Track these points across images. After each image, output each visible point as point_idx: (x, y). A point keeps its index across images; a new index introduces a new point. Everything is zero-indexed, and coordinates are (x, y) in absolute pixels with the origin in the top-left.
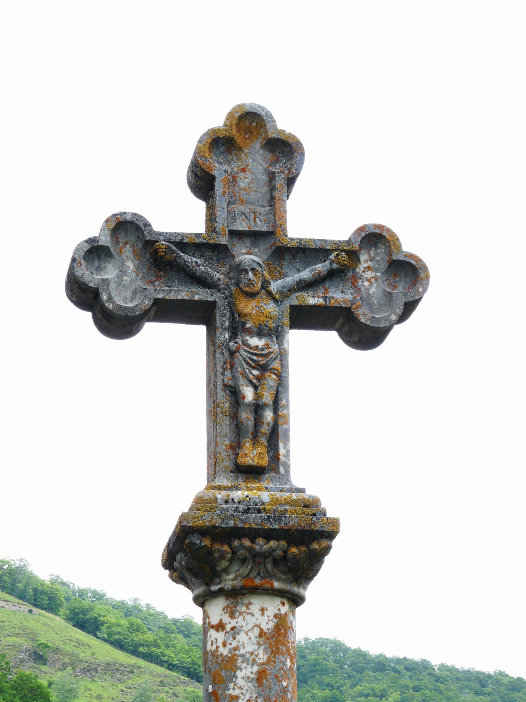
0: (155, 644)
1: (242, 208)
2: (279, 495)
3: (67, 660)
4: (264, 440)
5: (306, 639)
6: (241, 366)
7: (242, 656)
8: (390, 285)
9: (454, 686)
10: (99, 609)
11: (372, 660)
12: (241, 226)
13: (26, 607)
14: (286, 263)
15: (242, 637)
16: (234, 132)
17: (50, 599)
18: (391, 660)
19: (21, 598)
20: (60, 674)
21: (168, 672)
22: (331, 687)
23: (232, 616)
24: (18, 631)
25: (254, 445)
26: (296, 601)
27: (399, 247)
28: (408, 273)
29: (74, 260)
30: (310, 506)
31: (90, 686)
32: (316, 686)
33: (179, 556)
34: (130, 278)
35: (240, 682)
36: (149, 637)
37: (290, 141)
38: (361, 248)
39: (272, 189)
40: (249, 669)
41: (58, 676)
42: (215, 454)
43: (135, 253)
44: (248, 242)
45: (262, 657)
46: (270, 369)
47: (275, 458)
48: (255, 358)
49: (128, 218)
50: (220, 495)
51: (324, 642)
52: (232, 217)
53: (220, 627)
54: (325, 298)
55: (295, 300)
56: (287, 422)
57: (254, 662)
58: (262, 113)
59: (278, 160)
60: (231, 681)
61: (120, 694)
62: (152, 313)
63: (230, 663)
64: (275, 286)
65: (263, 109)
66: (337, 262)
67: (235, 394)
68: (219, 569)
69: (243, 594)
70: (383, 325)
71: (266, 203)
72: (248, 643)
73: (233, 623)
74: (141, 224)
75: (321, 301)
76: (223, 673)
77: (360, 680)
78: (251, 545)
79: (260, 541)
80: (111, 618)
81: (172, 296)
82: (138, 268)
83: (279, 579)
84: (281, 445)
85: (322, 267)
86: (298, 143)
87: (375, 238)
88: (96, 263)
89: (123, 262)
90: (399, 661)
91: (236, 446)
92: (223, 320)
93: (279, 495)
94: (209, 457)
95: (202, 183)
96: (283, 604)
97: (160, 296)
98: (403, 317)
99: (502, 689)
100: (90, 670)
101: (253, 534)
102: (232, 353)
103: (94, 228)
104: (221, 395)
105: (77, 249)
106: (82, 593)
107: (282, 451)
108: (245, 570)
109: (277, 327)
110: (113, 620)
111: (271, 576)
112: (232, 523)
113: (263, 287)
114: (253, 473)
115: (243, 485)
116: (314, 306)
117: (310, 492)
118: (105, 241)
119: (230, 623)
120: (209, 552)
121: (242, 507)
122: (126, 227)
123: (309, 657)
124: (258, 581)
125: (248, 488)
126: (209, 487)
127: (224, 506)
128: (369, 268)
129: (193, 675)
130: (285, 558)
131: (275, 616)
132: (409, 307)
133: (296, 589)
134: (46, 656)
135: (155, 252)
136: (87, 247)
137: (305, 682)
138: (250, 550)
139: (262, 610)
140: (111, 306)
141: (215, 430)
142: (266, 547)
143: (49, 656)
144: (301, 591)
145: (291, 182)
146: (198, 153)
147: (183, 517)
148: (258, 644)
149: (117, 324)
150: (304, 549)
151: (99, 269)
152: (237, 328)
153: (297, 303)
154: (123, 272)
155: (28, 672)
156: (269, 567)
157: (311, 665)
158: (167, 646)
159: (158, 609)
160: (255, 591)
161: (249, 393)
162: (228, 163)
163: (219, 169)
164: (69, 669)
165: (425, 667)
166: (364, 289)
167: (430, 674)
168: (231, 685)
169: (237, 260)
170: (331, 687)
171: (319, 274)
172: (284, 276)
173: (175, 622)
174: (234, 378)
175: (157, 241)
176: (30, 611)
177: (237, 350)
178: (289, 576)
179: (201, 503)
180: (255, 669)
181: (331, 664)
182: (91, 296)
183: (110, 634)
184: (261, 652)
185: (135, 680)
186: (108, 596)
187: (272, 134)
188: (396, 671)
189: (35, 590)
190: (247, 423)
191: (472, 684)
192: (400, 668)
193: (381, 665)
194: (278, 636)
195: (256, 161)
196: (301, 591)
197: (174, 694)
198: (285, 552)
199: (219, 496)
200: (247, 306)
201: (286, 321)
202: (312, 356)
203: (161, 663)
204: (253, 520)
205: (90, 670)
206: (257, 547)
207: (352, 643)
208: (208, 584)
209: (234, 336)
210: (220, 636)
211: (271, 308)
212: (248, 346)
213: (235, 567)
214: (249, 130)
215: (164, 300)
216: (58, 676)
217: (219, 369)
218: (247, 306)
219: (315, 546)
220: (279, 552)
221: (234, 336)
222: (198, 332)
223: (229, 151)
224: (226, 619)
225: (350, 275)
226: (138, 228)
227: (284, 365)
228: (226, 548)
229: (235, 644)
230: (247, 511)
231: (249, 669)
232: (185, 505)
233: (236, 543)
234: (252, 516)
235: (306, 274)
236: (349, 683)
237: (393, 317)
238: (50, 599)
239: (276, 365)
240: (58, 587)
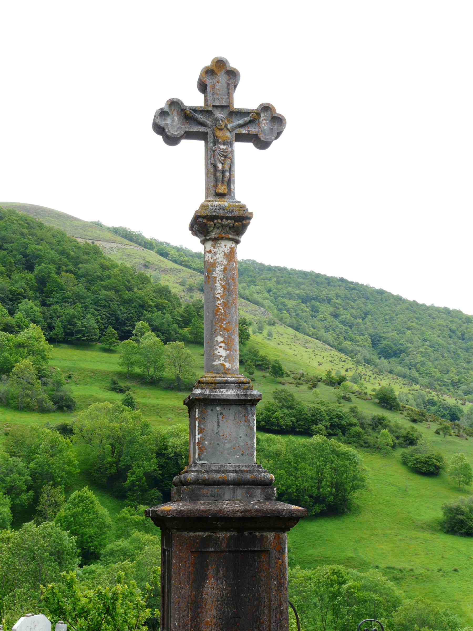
0: (188, 261)
1: (217, 96)
2: (231, 203)
3: (156, 267)
4: (226, 183)
5: (242, 259)
6: (217, 156)
7: (218, 262)
8: (272, 126)
9: (296, 276)
10: (168, 249)
11: (266, 267)
12: (217, 103)
13: (142, 248)
14: (233, 117)
15: (218, 255)
16: (214, 68)
17: (150, 245)
18: (273, 267)
19: (140, 245)
20: (154, 272)
21: (193, 271)
22: (251, 276)
23: (214, 248)
24: (139, 257)
25: (222, 185)
26: (237, 242)
27: (275, 112)
28: (278, 121)
29: (155, 116)
30: (243, 207)
31: (165, 277)
32: (246, 276)
33: (195, 226)
34: (176, 123)
35: (217, 272)
36: (186, 259)
37: (235, 71)
38: (261, 112)
39: (229, 89)
40: (221, 267)
41: (153, 273)
42: (208, 188)
43: (177, 113)
44: (219, 109)
45: (225, 263)
46: (228, 157)
47: (230, 190)
48: (222, 153)
49: (175, 100)
50: (210, 204)
51: (249, 260)
52: (214, 100)
53: (210, 252)
54: (248, 131)
55: (237, 131)
56: (234, 177)
57: (222, 264)
58: (225, 60)
59: (230, 78)
60: (214, 271)
61: (176, 279)
62: (184, 136)
63: (213, 265)
64: (229, 126)
65: (225, 59)
66: (252, 117)
67: (215, 166)
68: (209, 231)
69: (218, 240)
70: (269, 140)
71: (226, 95)
72: (220, 257)
73: (215, 250)
74: (180, 103)
75: (247, 132)
76: (211, 268)
77: (262, 274)
78: (221, 222)
79: (224, 220)
80: (173, 252)
81: (192, 130)
82: (179, 119)
83: (231, 234)
84: (232, 185)
85: (247, 119)
86: (238, 72)
87: (266, 108)
88: (164, 117)
89: (173, 117)
90: (276, 267)
91: (216, 186)
92: (210, 139)
93: (231, 203)
94: (206, 190)
95: (203, 87)
96: (233, 243)
97: (187, 130)
98: (277, 138)
99: (313, 277)
100: (165, 271)
101: (222, 218)
102: (214, 151)
103: (162, 104)
104: (211, 167)
105: (156, 112)
106: (162, 243)
107: (232, 187)
108: (219, 231)
109: (231, 141)
110: (173, 253)
111: (228, 233)
112: (214, 214)
113: (225, 126)
114: (221, 195)
115: (218, 200)
116: (244, 134)
117: (242, 202)
118: (167, 109)
119: (214, 250)
120: (206, 225)
121: (218, 208)
122: (174, 104)
123: (244, 266)
124: (223, 235)
125: (220, 201)
126: (206, 201)
127: (211, 208)
128: (264, 119)
129: (202, 273)
130: (233, 227)
131: (230, 248)
132: (279, 134)
133: (237, 238)
134: (149, 266)
135: (185, 113)
136: (160, 111)
137: (242, 275)
138: (220, 224)
139: (225, 246)
140: (169, 134)
141: (208, 180)
142: (227, 223)
143: (150, 266)
144: (239, 239)
145: (235, 87)
146: (201, 76)
147: (197, 212)
148: (224, 258)
149: (172, 140)
150: (240, 223)
151: (164, 120)
152: (216, 142)
153: (238, 132)
154: (173, 121)
155: (143, 272)
156: (228, 230)
157: (245, 269)
158: (193, 262)
159: (189, 249)
160: (222, 238)
161: (220, 166)
162: (212, 79)
163: (209, 82)
164: (157, 270)
165: (285, 269)
166: (262, 126)
167: (287, 272)
168: (214, 273)
169: (215, 116)
170: (251, 276)
171: (246, 121)
172: (233, 122)
173: (195, 253)
174: (215, 160)
175: (185, 109)
176: (143, 250)
177: (216, 150)
178: (235, 233)
179: (203, 207)
180: (223, 267)
181: (252, 268)
182: (162, 130)
183: (172, 258)
184: (225, 261)
185: (181, 274)
186: (171, 244)
187: (228, 69)
188: (275, 271)
189: (145, 242)
190: (220, 177)
191: (301, 275)
192: (276, 270)
193: (269, 269)
194: (231, 255)
195: (222, 78)
196: (239, 239)
197: (195, 279)
198: (234, 225)
199: (209, 204)
200: (219, 134)
201: (234, 139)
202: (243, 151)
203: (190, 268)
204: (222, 213)
205: (165, 271)
206: (223, 223)
207: (259, 261)
208: (205, 236)
209: (214, 145)
210: (210, 255)
211: (228, 134)
212: (220, 148)
213: (215, 230)
214: (219, 67)
215: (188, 131)
216: (153, 273)
217: (209, 157)
218: (219, 134)
219: (244, 222)
220: (231, 225)
221: (214, 145)
222: (202, 143)
223: (212, 75)
224: (212, 249)
225: (257, 122)
226: (179, 104)
227: (233, 156)
228: (212, 223)
229: (215, 258)
230: (220, 209)
231: (221, 267)
232: (197, 207)
233: (216, 221)
234: (221, 211)
235: (241, 122)
236: (258, 275)
237: (273, 138)
238: (150, 245)
239: (230, 155)
240: (153, 241)
